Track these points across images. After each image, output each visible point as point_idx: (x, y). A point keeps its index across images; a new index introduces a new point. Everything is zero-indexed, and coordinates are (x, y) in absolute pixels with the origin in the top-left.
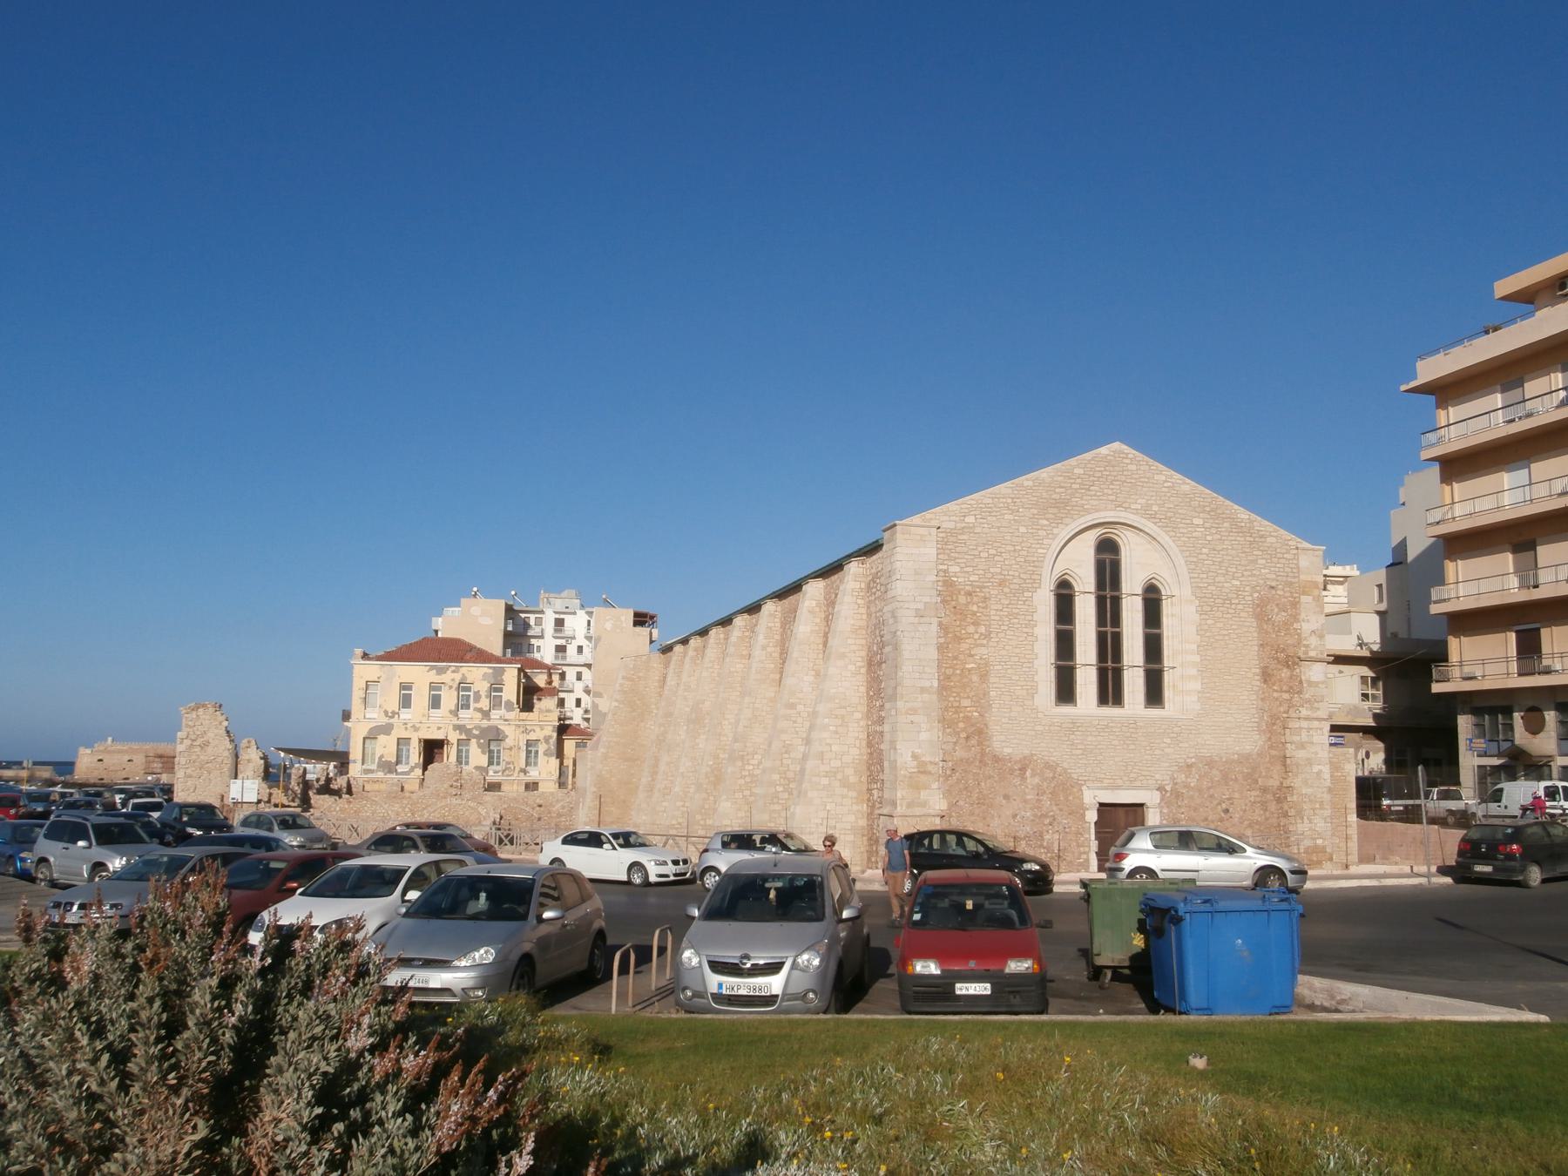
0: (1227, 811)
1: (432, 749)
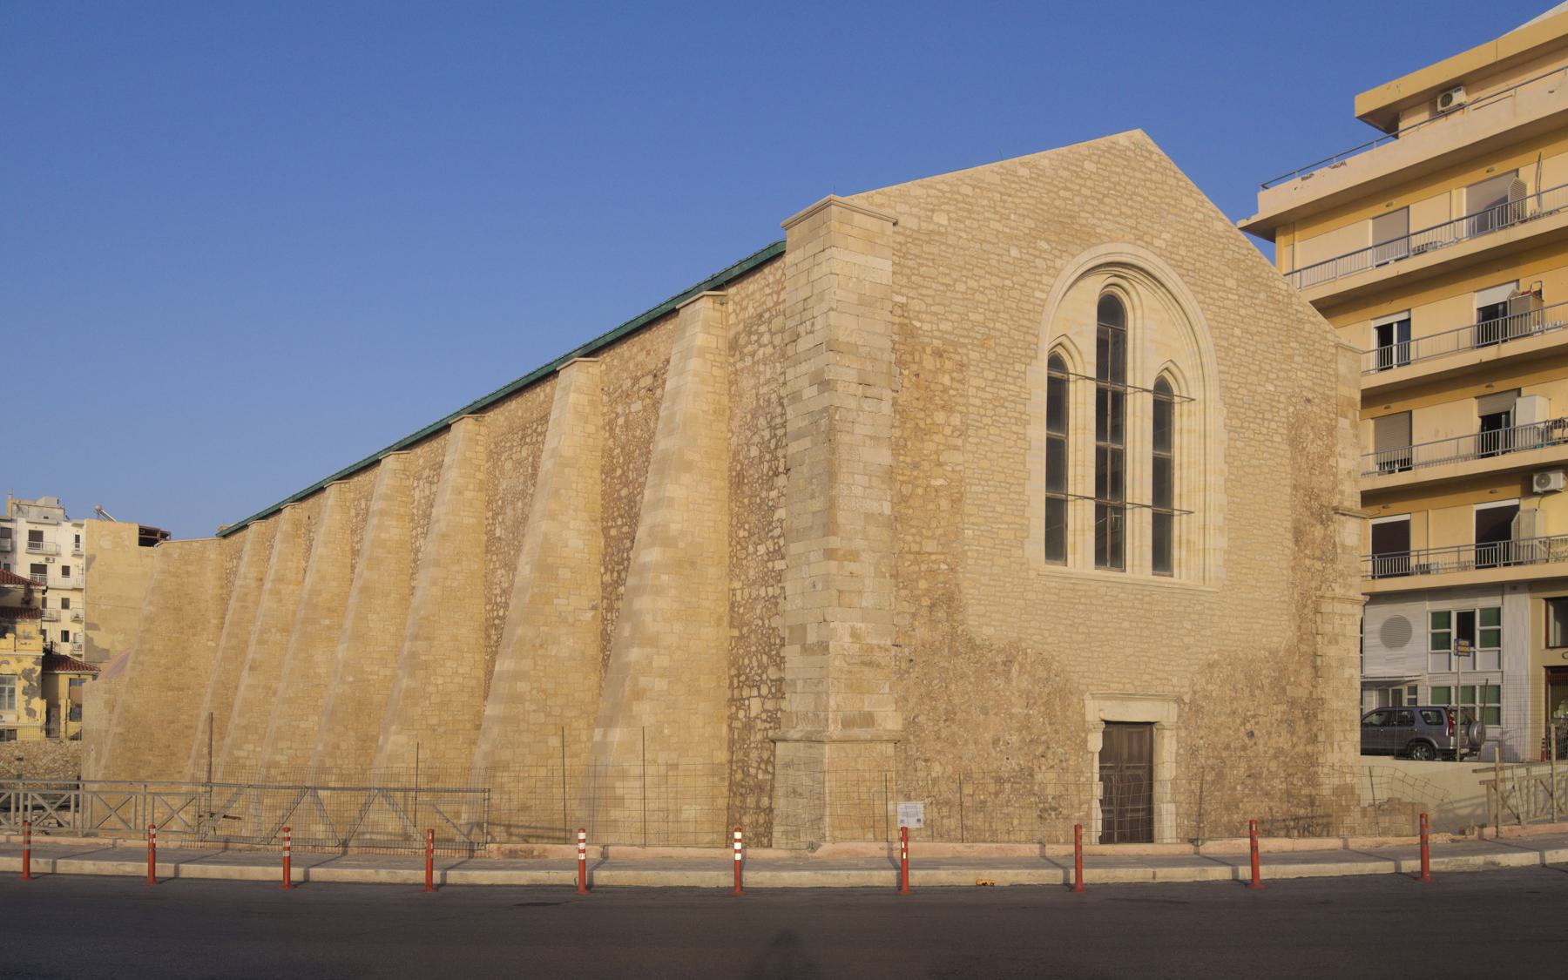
0: (1251, 734)
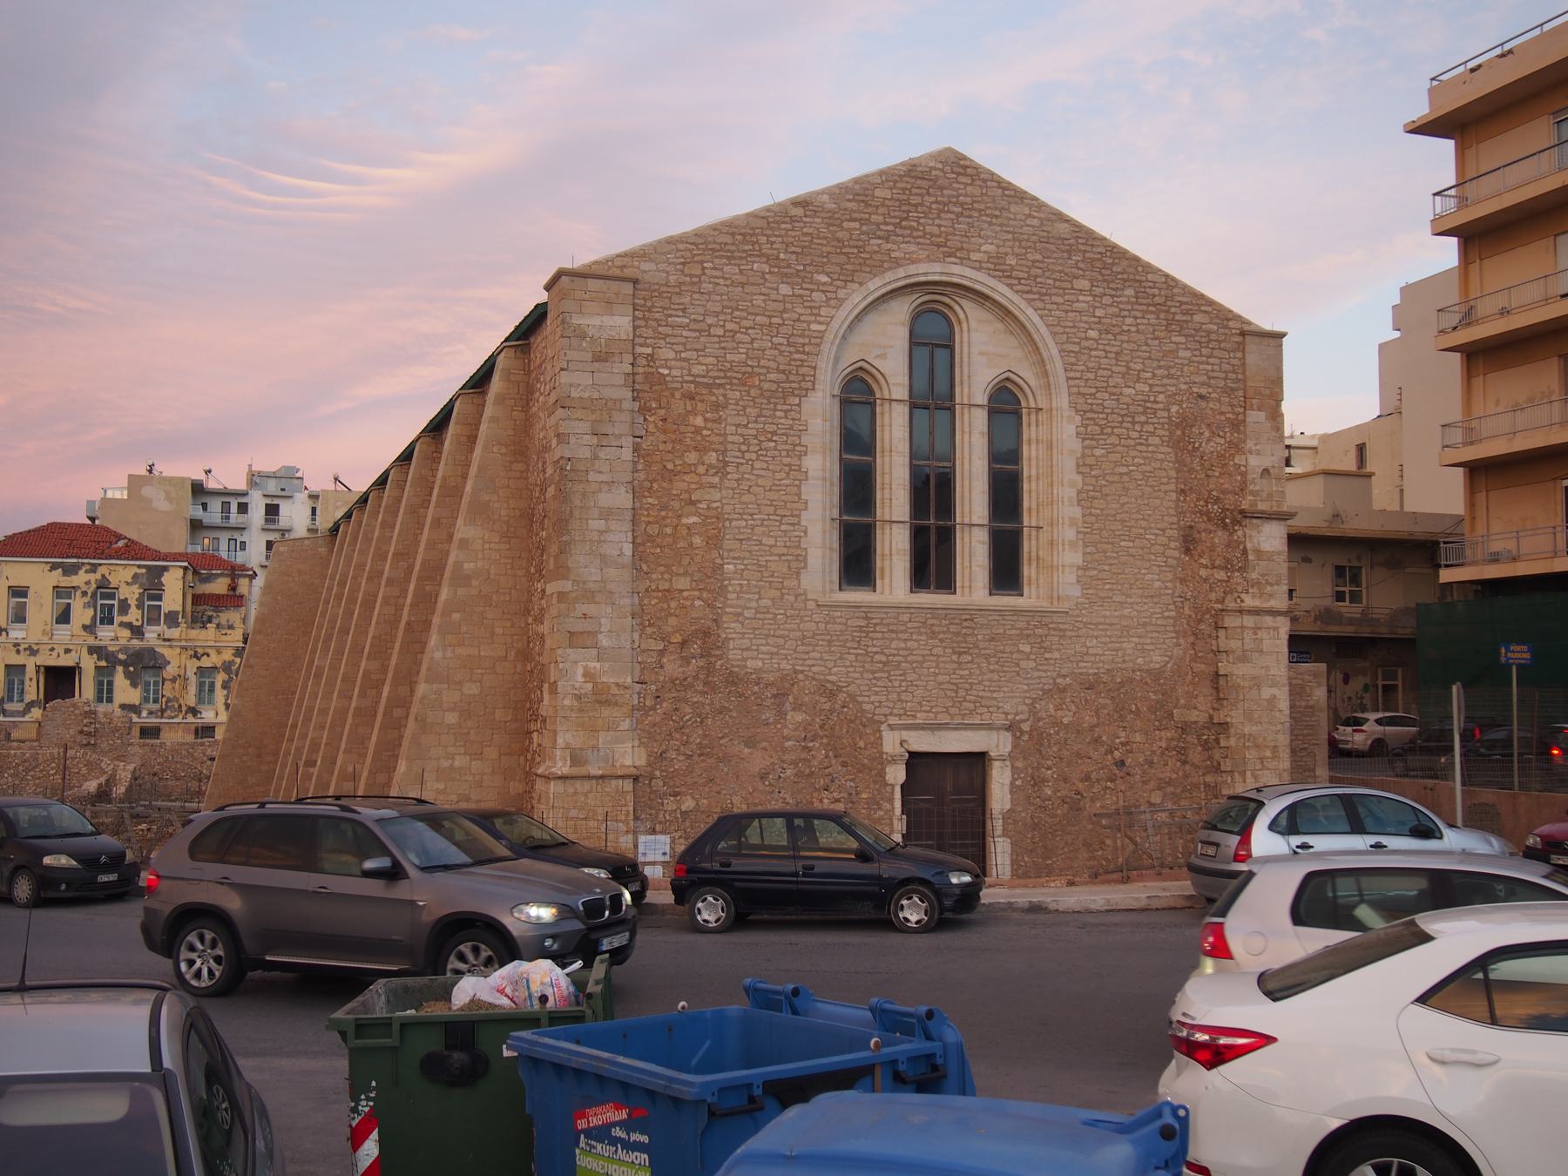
1: (60, 681)
